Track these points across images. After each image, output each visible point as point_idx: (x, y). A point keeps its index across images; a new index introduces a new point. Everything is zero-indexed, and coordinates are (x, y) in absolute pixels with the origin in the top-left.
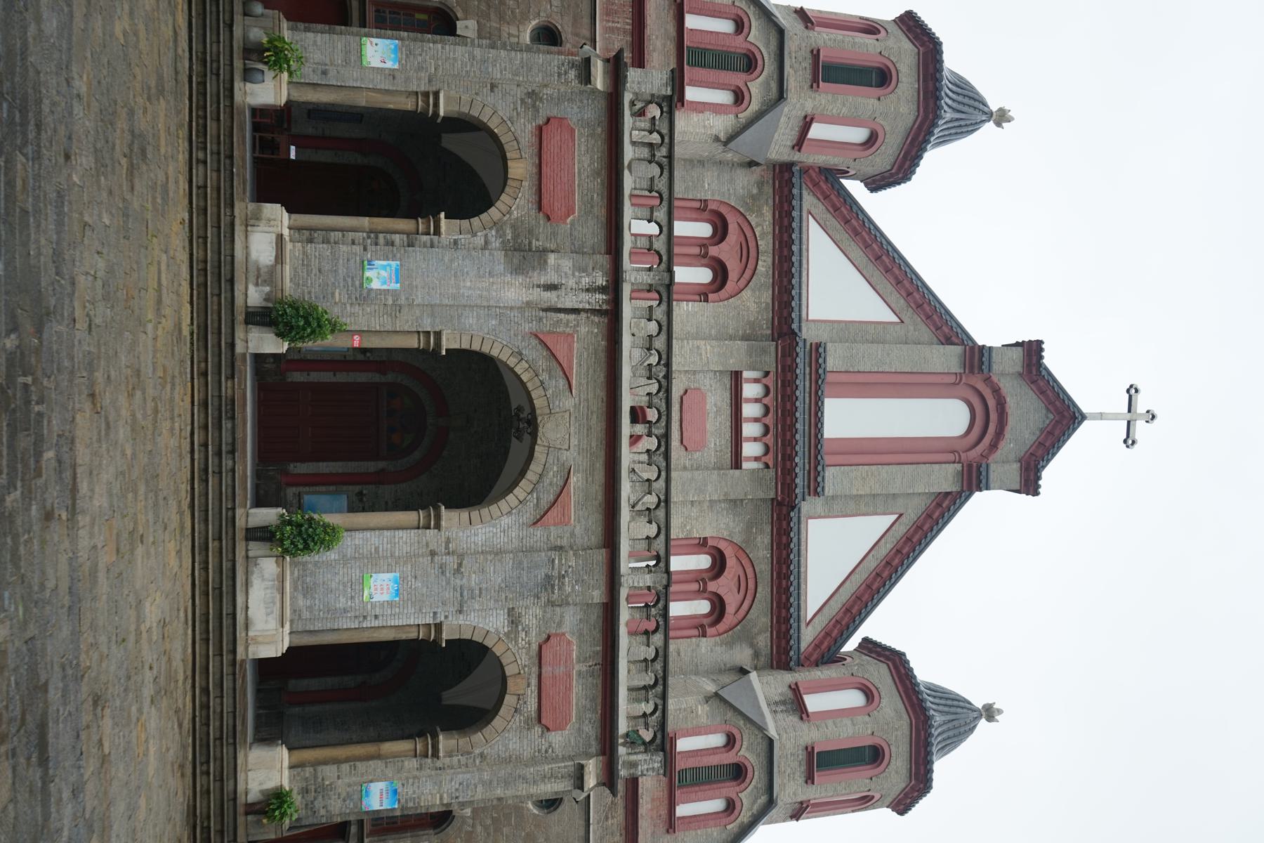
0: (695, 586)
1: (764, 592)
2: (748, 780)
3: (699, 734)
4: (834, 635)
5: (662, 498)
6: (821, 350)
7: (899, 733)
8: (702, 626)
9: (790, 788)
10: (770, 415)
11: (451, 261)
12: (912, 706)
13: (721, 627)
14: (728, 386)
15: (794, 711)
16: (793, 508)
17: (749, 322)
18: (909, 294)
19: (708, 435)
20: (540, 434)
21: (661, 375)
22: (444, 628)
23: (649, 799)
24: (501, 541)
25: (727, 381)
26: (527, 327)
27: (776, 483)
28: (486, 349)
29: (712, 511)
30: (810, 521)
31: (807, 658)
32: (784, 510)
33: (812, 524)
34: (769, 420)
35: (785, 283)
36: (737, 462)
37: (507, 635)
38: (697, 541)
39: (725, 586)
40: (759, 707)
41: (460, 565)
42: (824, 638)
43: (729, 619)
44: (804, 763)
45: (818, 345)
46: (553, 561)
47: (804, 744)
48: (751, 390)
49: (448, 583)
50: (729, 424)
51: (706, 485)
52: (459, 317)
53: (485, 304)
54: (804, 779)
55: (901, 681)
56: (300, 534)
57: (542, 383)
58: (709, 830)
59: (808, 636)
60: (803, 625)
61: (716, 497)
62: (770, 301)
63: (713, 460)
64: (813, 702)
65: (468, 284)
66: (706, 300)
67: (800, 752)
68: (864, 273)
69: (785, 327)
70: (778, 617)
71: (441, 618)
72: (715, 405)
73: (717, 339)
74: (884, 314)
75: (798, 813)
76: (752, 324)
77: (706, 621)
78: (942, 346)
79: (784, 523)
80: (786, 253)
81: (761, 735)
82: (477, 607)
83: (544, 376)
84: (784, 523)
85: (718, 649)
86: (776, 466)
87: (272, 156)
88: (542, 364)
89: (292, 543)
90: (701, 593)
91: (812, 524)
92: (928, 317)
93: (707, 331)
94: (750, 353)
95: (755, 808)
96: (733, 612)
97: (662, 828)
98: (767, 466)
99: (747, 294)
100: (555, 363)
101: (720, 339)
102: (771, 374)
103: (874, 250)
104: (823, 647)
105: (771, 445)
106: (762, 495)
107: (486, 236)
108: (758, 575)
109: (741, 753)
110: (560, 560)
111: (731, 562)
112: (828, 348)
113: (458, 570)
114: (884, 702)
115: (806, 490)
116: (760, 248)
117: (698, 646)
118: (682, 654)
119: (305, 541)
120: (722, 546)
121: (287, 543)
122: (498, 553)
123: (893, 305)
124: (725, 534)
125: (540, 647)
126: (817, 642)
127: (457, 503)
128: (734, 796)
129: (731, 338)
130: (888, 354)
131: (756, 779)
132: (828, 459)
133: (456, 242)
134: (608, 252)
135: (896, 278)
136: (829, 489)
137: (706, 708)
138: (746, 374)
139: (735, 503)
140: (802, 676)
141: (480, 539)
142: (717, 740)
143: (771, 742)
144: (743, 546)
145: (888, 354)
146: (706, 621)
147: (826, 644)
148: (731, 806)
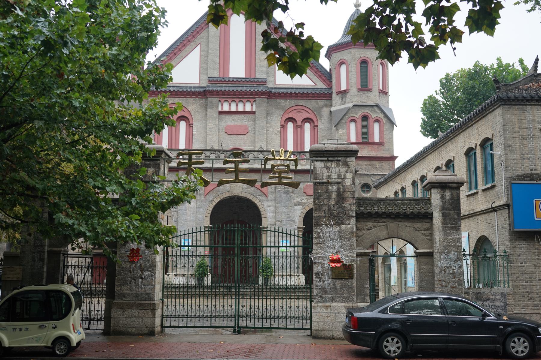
0: (299, 130)
1: (302, 102)
2: (368, 114)
3: (349, 133)
4: (320, 74)
5: (260, 153)
6: (211, 79)
7: (356, 53)
8: (314, 126)
9: (373, 98)
10: (235, 100)
11: (182, 223)
12: (347, 47)
13: (314, 119)
14: (224, 116)
15: (345, 95)
16: (270, 92)
17: (200, 108)
18: (189, 41)
19: (242, 124)
20: (238, 195)
21: (218, 153)
22: (299, 226)
23: (371, 152)
24: (272, 208)
25: (222, 116)
26: (203, 199)
27: (261, 98)
28: (210, 212)
29: (271, 123)
30: (276, 83)
31: (329, 85)
32: (271, 95)
33: (277, 82)
34: (237, 100)
35: (185, 93)
36: (253, 113)
37: (303, 206)
38: (282, 129)
39: (299, 118)
40: (342, 109)
41: (279, 221)
42: (321, 78)
43: (312, 116)
44: (364, 92)
45: (209, 81)
46: (279, 191)
47: (357, 92)
48: (226, 108)
49: (285, 225)
50: (238, 116)
51: (261, 126)
52: (199, 220)
53: (195, 212)
54: (370, 92)
55: (338, 49)
56: (266, 270)
57: (221, 194)
58: (385, 129)
59: (320, 85)
60: (316, 87)
61: (265, 122)
62: (192, 99)
63: (252, 122)
64: (344, 87)
65: (189, 218)
66: (192, 124)
67: (360, 94)
68: (181, 60)
69: (202, 94)
70: (312, 97)
71: (296, 227)
72: (231, 121)
73: (207, 121)
74: (197, 50)
75: (384, 93)
76: (201, 106)
77: (312, 125)
78: (210, 27)
79: (276, 95)
80: (174, 93)
81: (352, 109)
82: (293, 216)
83: (219, 193)
84: (276, 95)
85: (323, 121)
86: (255, 98)
87: (437, 216)
88: (214, 194)
89: (268, 272)
90: (302, 127)
91: (277, 82)
92: (198, 33)
93: (204, 124)
94: (212, 108)
95: (379, 111)
96: (309, 114)
97: (382, 147)
98: (255, 101)
99: (190, 108)
100: (214, 189)
101: (207, 119)
102: (220, 99)
103: (172, 56)
104: (325, 79)
105: (247, 100)
106: (265, 103)
107: (173, 212)
108: (296, 105)
109: (357, 117)
110: (279, 188)
111: (290, 115)
112: (210, 76)
113: (281, 222)
114: (345, 58)
115: (264, 86)
116: (172, 103)
117: (321, 129)
118: (323, 135)
119: (268, 269)
120: (284, 119)
121: (268, 274)
122: (276, 209)
123: (193, 47)
124: (280, 118)
125: (307, 195)
126: (323, 81)
127: (260, 222)
128: (374, 120)
129: (206, 115)
130: (213, 51)
131: (368, 111)
132: (253, 77)
133: (175, 221)
134: (178, 171)
135: (183, 46)
136: (264, 76)
137: (340, 130)
138: (220, 109)
139: (268, 114)
140: (334, 90)
141: (271, 215)
142: (353, 126)
143: (354, 105)
144: (284, 111)
145: (213, 51)
146: (312, 125)
147: (323, 78)
148: (377, 121)
